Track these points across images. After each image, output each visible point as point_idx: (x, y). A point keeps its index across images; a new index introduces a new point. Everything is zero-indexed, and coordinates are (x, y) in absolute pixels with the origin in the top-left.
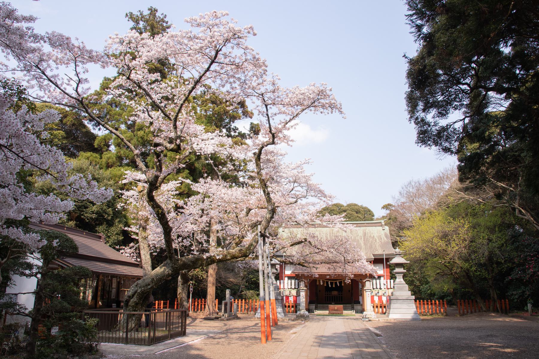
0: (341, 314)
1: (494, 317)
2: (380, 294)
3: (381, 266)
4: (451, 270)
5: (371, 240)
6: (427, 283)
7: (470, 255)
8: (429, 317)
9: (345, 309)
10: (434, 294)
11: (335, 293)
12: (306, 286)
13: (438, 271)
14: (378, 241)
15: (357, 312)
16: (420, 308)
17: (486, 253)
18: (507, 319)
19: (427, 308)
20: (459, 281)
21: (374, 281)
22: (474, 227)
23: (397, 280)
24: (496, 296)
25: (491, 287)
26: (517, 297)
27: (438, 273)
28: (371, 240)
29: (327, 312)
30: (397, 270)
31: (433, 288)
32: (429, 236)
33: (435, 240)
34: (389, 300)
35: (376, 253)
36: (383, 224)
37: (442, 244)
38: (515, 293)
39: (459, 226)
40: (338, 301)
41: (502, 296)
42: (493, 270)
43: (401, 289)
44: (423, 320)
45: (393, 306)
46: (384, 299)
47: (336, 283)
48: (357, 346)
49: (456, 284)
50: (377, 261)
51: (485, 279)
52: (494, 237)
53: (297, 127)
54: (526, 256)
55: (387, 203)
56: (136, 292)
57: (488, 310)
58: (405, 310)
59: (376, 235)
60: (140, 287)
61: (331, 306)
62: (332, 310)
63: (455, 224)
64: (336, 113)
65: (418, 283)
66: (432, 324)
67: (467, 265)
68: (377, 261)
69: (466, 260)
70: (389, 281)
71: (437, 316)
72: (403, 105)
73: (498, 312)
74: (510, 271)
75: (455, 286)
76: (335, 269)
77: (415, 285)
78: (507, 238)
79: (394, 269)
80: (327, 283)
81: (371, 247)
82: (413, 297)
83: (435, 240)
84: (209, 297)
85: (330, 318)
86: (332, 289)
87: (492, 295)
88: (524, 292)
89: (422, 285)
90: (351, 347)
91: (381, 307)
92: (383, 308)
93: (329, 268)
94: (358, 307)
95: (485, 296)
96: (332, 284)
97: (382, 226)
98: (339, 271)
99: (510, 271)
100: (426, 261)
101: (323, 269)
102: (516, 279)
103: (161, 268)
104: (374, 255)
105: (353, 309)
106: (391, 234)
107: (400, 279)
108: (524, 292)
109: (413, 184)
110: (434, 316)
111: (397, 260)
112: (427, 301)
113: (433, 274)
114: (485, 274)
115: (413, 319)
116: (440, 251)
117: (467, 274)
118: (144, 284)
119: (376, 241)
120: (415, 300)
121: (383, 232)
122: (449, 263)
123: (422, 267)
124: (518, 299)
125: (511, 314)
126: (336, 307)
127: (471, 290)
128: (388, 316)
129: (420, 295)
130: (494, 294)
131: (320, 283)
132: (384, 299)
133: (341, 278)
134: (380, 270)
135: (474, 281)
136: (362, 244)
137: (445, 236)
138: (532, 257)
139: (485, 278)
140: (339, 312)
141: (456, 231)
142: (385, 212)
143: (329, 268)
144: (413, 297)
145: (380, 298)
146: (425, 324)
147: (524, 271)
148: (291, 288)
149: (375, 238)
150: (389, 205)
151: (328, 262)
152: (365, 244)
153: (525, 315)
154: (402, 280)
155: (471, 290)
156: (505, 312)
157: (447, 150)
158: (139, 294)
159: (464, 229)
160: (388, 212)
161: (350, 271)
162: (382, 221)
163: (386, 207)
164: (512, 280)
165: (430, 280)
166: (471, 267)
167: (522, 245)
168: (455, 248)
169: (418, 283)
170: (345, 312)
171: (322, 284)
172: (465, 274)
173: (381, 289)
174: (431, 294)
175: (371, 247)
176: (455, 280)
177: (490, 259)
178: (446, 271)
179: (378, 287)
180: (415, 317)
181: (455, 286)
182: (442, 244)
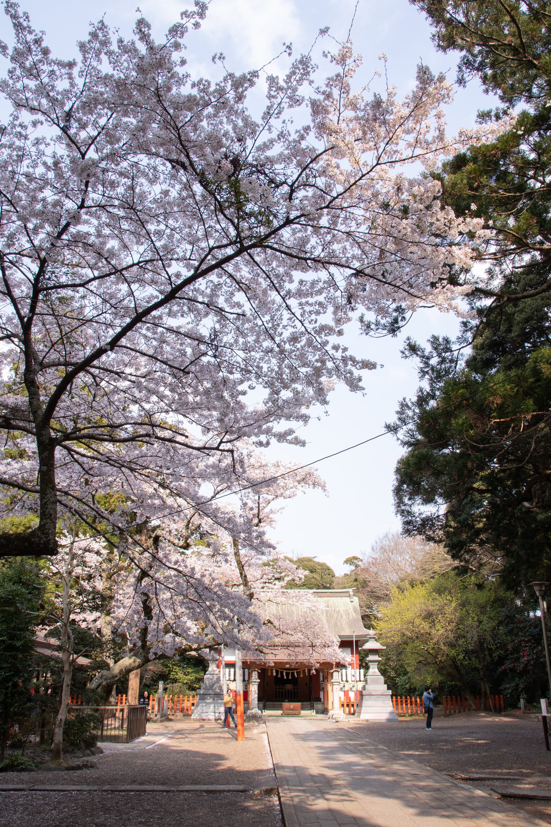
0: (297, 715)
1: (484, 717)
2: (346, 689)
3: (349, 650)
4: (436, 657)
5: (336, 615)
6: (406, 673)
7: (457, 640)
8: (408, 719)
9: (303, 708)
10: (415, 690)
11: (289, 687)
12: (259, 678)
13: (421, 659)
14: (344, 617)
15: (317, 713)
16: (397, 709)
17: (475, 639)
18: (497, 719)
19: (406, 708)
20: (445, 672)
21: (344, 671)
22: (463, 605)
23: (371, 671)
24: (488, 691)
25: (482, 679)
26: (510, 691)
27: (420, 662)
28: (336, 615)
29: (280, 712)
30: (371, 657)
31: (413, 680)
32: (409, 615)
33: (417, 621)
34: (361, 695)
35: (343, 634)
36: (352, 593)
37: (425, 626)
38: (508, 687)
39: (446, 604)
40: (293, 698)
41: (496, 691)
42: (484, 658)
43: (375, 682)
44: (401, 721)
45: (365, 703)
46: (352, 695)
47: (293, 674)
48: (341, 740)
49: (442, 675)
50: (345, 644)
51: (476, 669)
52: (484, 618)
53: (283, 511)
54: (520, 641)
55: (351, 556)
56: (100, 685)
57: (478, 709)
58: (379, 709)
59: (342, 609)
60: (106, 679)
61: (286, 704)
62: (287, 709)
63: (441, 600)
64: (319, 490)
65: (393, 674)
66: (412, 725)
67: (453, 651)
68: (345, 644)
69: (452, 645)
70: (358, 670)
71: (417, 717)
72: (391, 499)
73: (491, 710)
74: (501, 660)
75: (440, 678)
76: (297, 656)
77: (389, 676)
78: (500, 619)
79: (367, 656)
80: (282, 673)
81: (336, 625)
82: (390, 692)
83: (417, 621)
84: (130, 692)
85: (285, 719)
86: (288, 681)
87: (483, 690)
88: (517, 685)
89: (398, 675)
90: (336, 740)
91: (348, 705)
92: (352, 707)
93: (289, 655)
94: (319, 706)
95: (476, 692)
96: (287, 674)
97: (349, 596)
98: (300, 658)
99: (501, 660)
100: (405, 646)
101: (282, 656)
102: (510, 669)
103: (130, 658)
104: (340, 636)
105: (312, 708)
106: (361, 607)
107: (374, 670)
108: (517, 685)
109: (390, 537)
110: (414, 717)
111: (371, 645)
112: (406, 698)
113: (414, 662)
114: (475, 662)
115: (389, 720)
116: (422, 634)
117: (454, 662)
118: (110, 676)
119: (342, 617)
120: (392, 696)
121: (351, 605)
122: (433, 648)
123: (400, 653)
124: (511, 693)
125: (503, 713)
126: (292, 705)
127: (459, 684)
128: (359, 716)
129: (400, 690)
130: (486, 687)
131: (272, 673)
132: (352, 695)
133: (304, 667)
134: (347, 656)
135: (463, 672)
136: (325, 621)
137: (429, 616)
138: (527, 642)
139: (476, 668)
140: (295, 712)
141: (441, 610)
142: (348, 569)
143: (289, 655)
144: (390, 692)
145: (346, 693)
146: (404, 725)
147: (517, 659)
148: (229, 680)
149: (341, 612)
150: (355, 558)
151: (286, 646)
152: (328, 621)
153: (518, 713)
154: (377, 670)
155: (459, 684)
156: (498, 711)
157: (429, 539)
158: (104, 686)
159: (451, 607)
160: (353, 568)
161: (314, 658)
162: (350, 590)
163: (350, 561)
164: (505, 670)
165: (408, 669)
166: (458, 655)
167: (517, 628)
168: (440, 631)
169: (393, 674)
170: (303, 712)
171: (275, 674)
172: (451, 662)
173: (347, 681)
174: (411, 689)
175: (336, 625)
176: (441, 669)
177: (481, 642)
178: (428, 661)
179: (344, 679)
180: (391, 717)
181: (440, 678)
182: (425, 626)
